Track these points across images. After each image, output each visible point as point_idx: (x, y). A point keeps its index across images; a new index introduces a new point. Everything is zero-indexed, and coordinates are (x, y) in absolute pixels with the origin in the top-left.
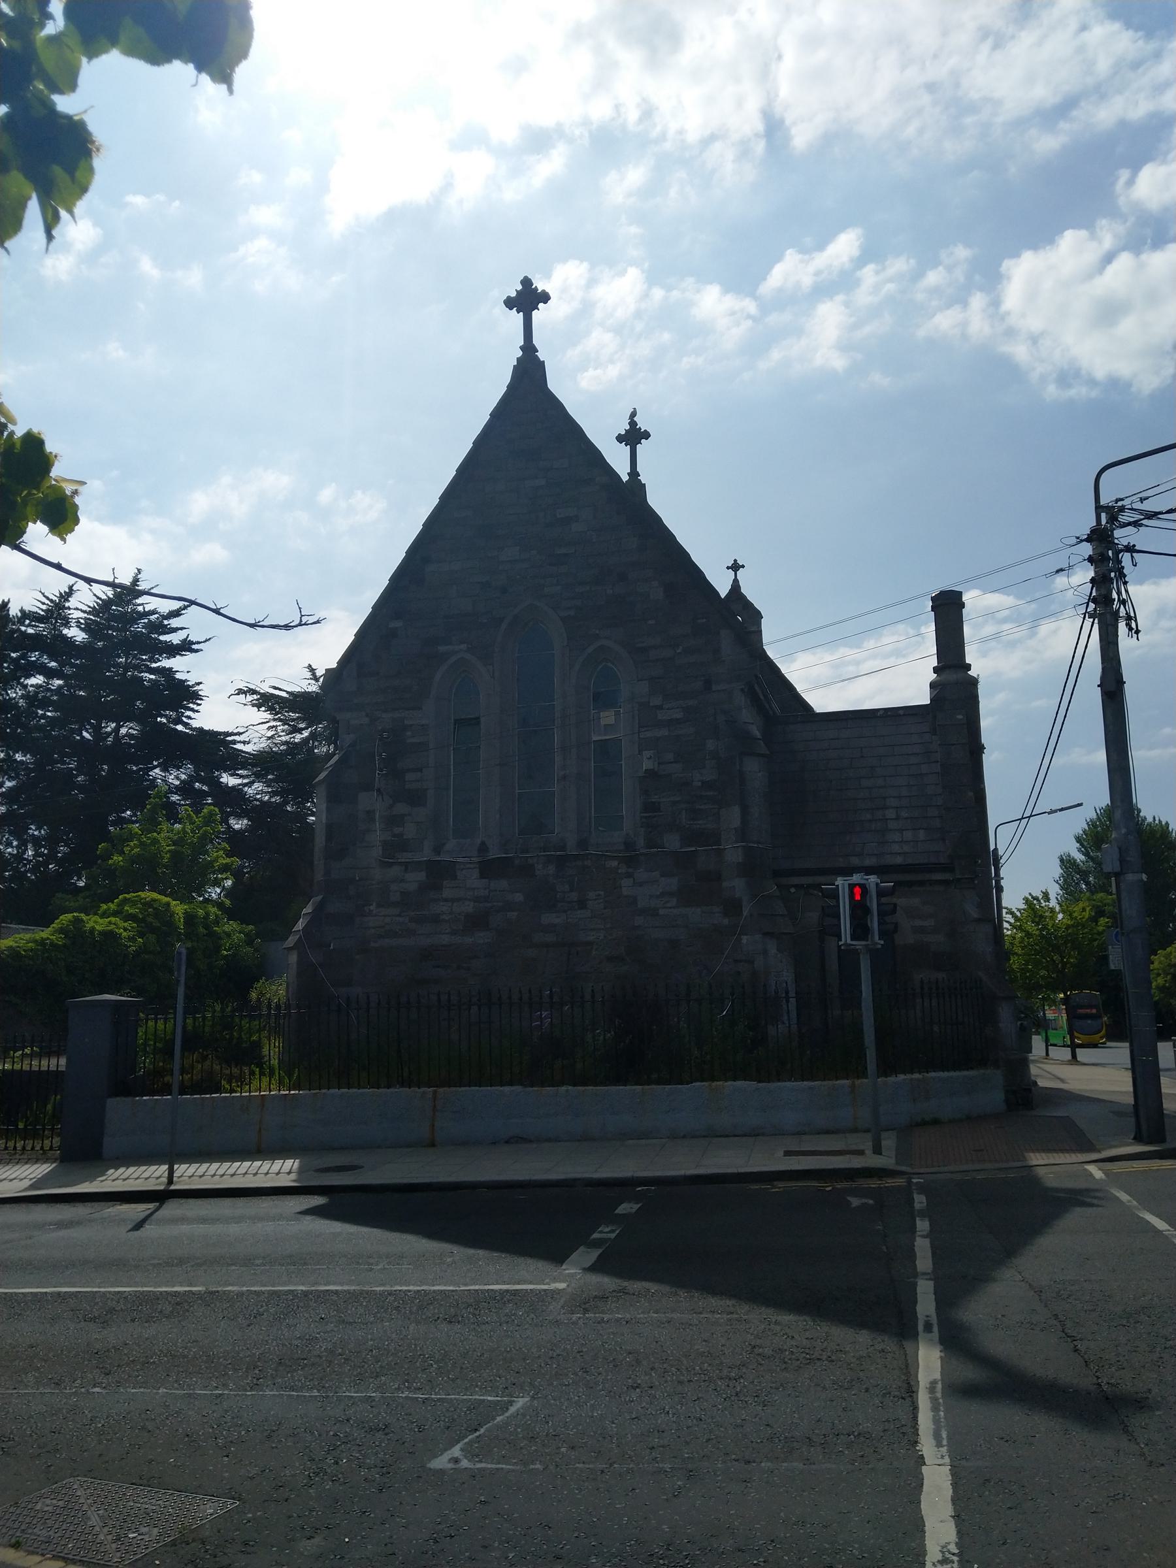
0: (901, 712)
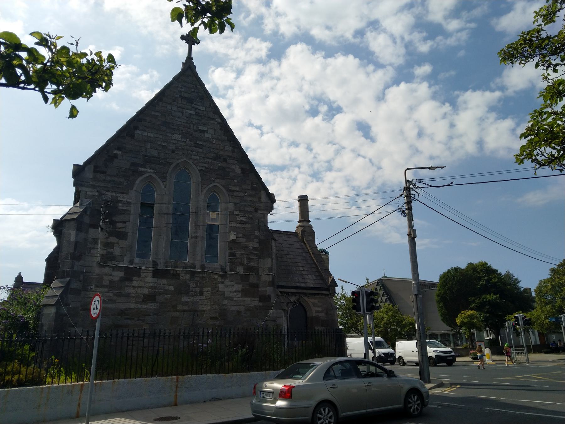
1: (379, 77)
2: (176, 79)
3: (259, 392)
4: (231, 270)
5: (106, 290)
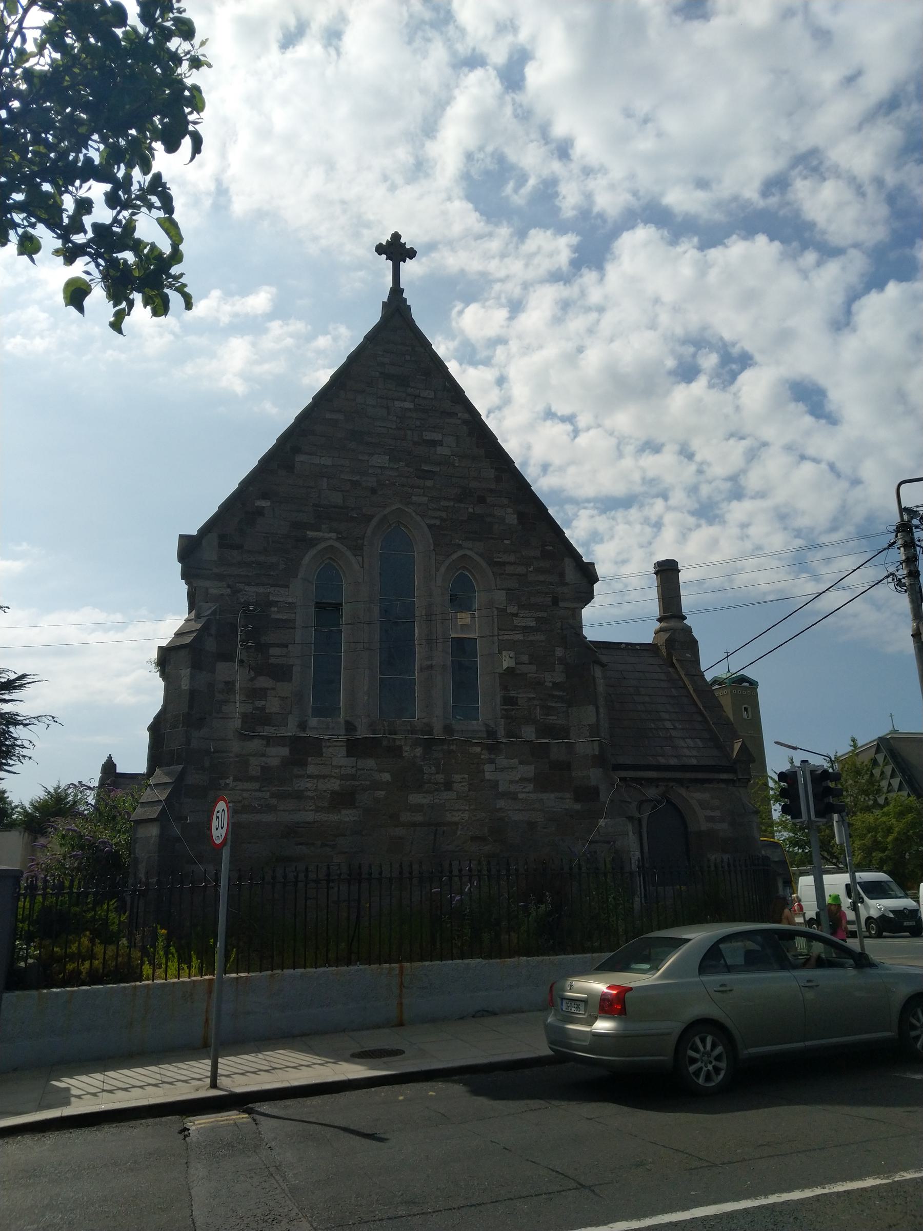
0: (638, 647)
1: (831, 277)
2: (372, 338)
3: (559, 1000)
4: (510, 734)
5: (255, 785)
